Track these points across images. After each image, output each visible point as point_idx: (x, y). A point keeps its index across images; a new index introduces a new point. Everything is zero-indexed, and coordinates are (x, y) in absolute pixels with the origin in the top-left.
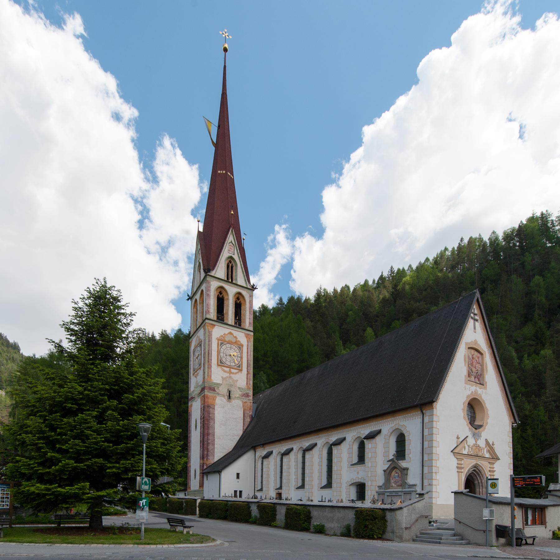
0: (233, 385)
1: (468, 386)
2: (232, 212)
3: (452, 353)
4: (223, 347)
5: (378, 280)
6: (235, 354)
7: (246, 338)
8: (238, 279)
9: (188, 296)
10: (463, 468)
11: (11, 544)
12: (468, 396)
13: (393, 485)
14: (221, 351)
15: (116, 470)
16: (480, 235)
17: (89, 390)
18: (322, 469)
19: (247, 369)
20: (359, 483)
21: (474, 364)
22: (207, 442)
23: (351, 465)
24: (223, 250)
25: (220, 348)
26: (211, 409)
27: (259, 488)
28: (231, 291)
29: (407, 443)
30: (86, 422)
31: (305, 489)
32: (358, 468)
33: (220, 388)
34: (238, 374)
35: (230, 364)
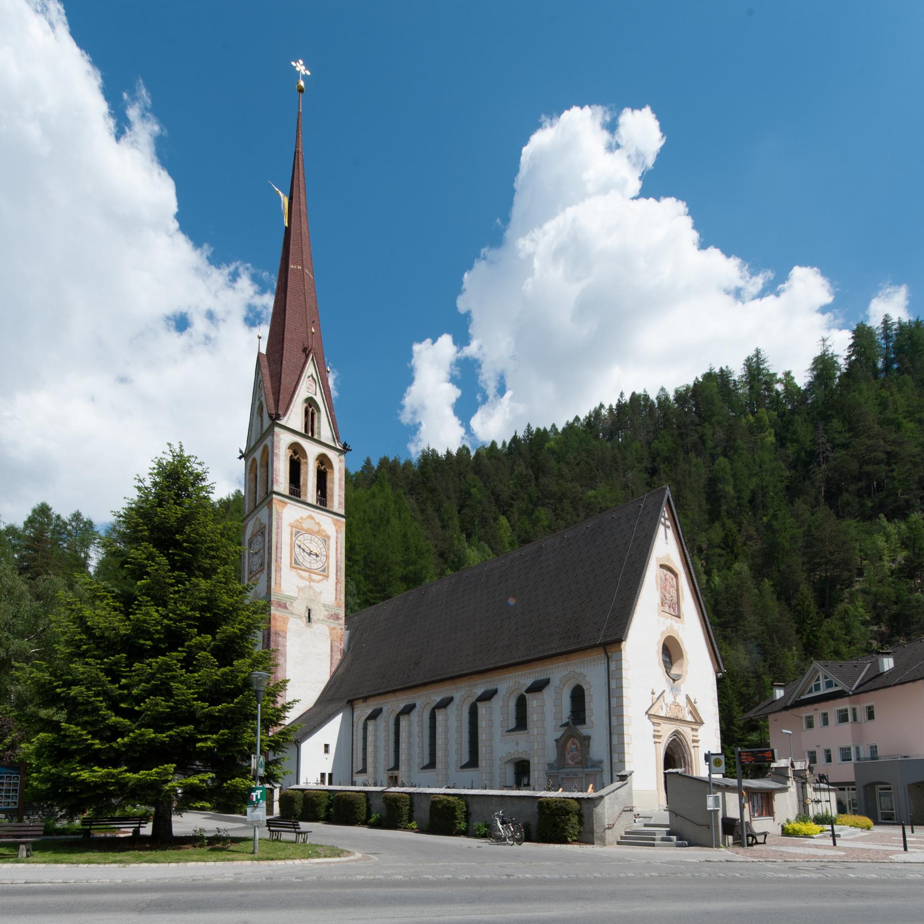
1: (662, 619)
3: (642, 573)
5: (510, 443)
8: (322, 433)
9: (241, 452)
10: (661, 736)
11: (58, 865)
12: (663, 633)
13: (570, 762)
15: (212, 743)
16: (645, 391)
17: (171, 619)
18: (461, 738)
19: (337, 575)
20: (519, 760)
21: (668, 587)
23: (507, 732)
25: (294, 539)
26: (280, 639)
27: (360, 768)
28: (312, 450)
29: (587, 699)
30: (169, 668)
31: (480, 768)
33: (294, 604)
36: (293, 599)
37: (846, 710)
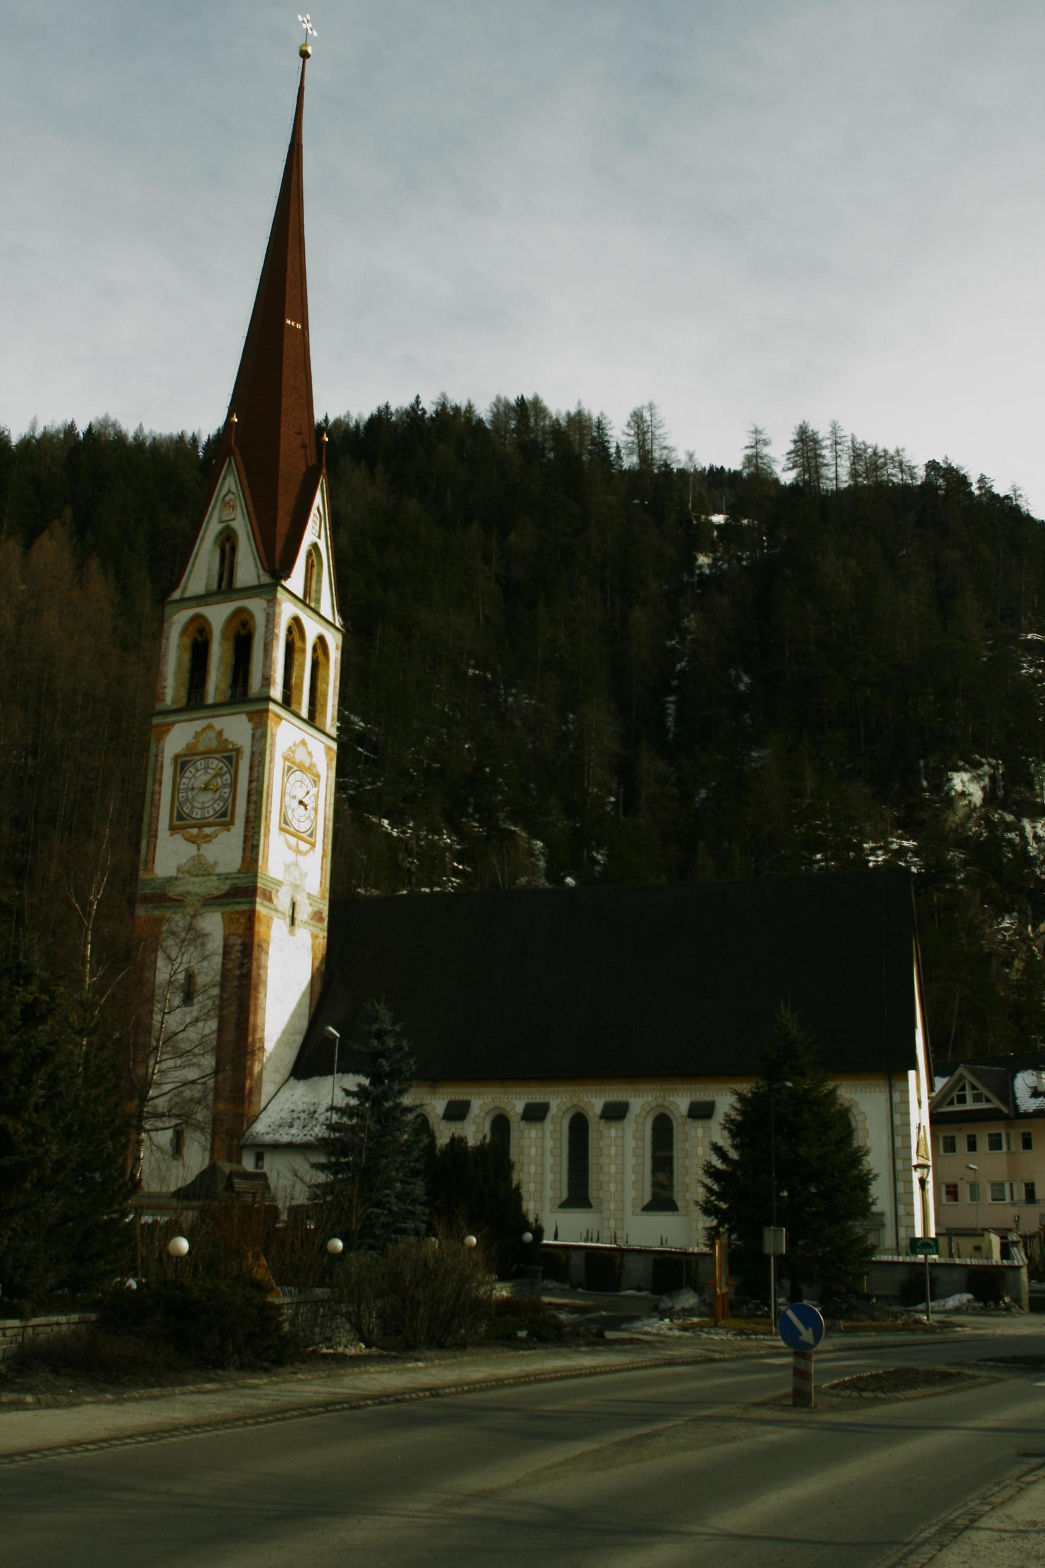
19: (324, 842)
28: (313, 629)
36: (279, 883)
37: (999, 1135)
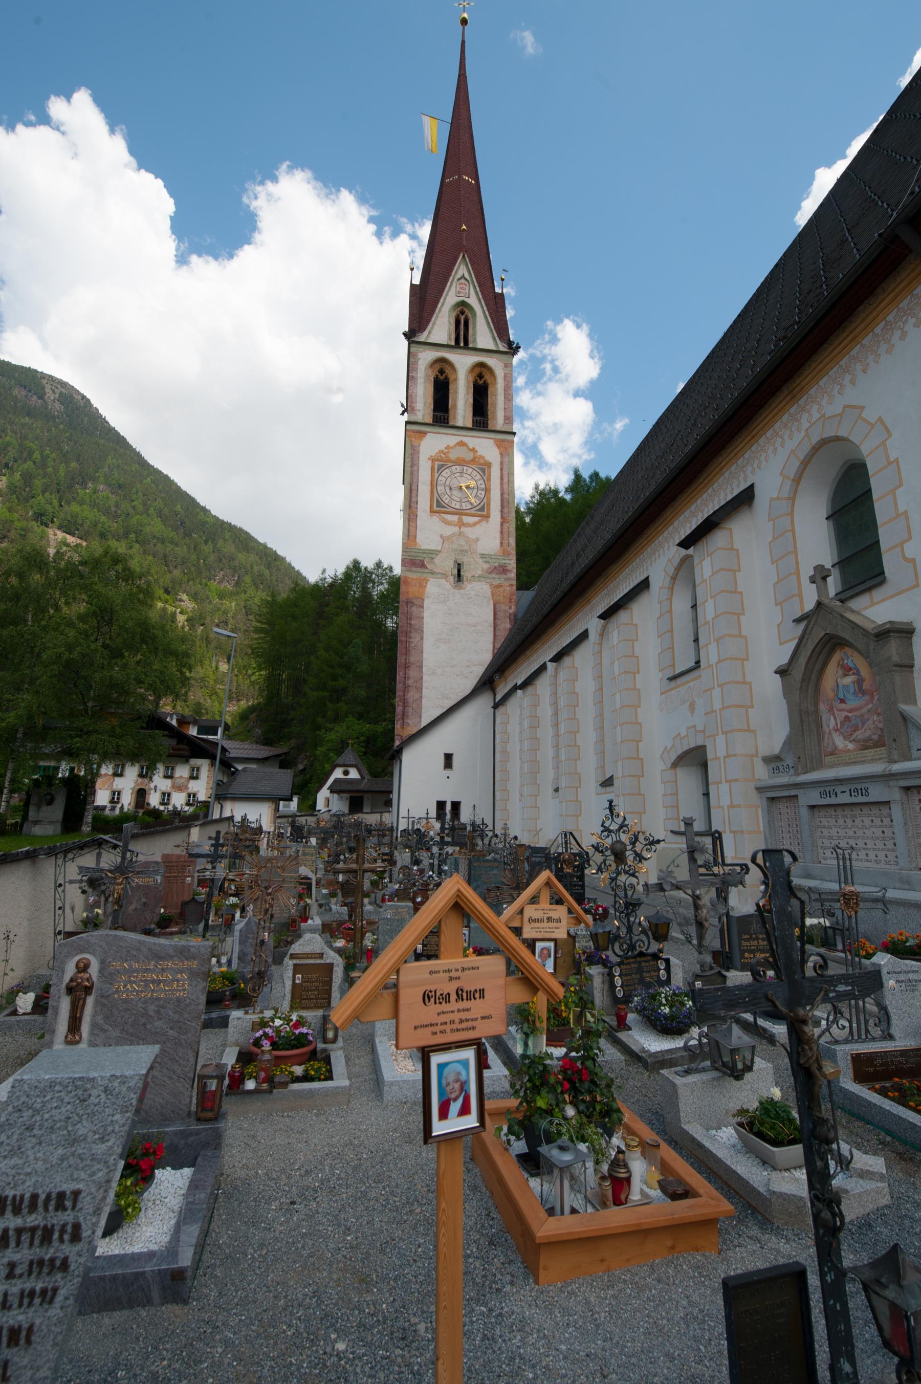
0: (466, 551)
2: (464, 227)
4: (444, 473)
6: (473, 484)
7: (499, 447)
9: (402, 405)
13: (840, 742)
14: (439, 482)
19: (502, 511)
22: (405, 683)
24: (445, 293)
25: (436, 475)
26: (414, 609)
28: (463, 362)
32: (691, 684)
33: (436, 561)
34: (478, 526)
35: (461, 505)
